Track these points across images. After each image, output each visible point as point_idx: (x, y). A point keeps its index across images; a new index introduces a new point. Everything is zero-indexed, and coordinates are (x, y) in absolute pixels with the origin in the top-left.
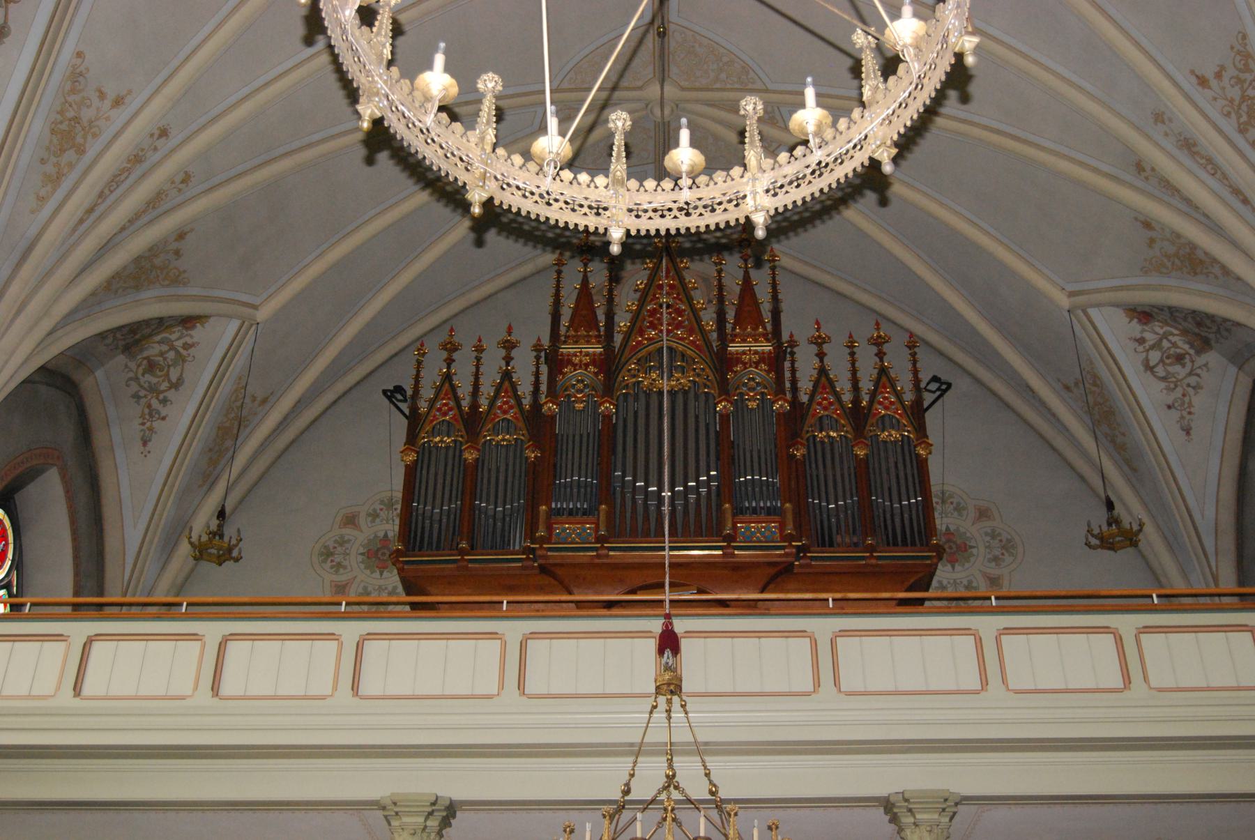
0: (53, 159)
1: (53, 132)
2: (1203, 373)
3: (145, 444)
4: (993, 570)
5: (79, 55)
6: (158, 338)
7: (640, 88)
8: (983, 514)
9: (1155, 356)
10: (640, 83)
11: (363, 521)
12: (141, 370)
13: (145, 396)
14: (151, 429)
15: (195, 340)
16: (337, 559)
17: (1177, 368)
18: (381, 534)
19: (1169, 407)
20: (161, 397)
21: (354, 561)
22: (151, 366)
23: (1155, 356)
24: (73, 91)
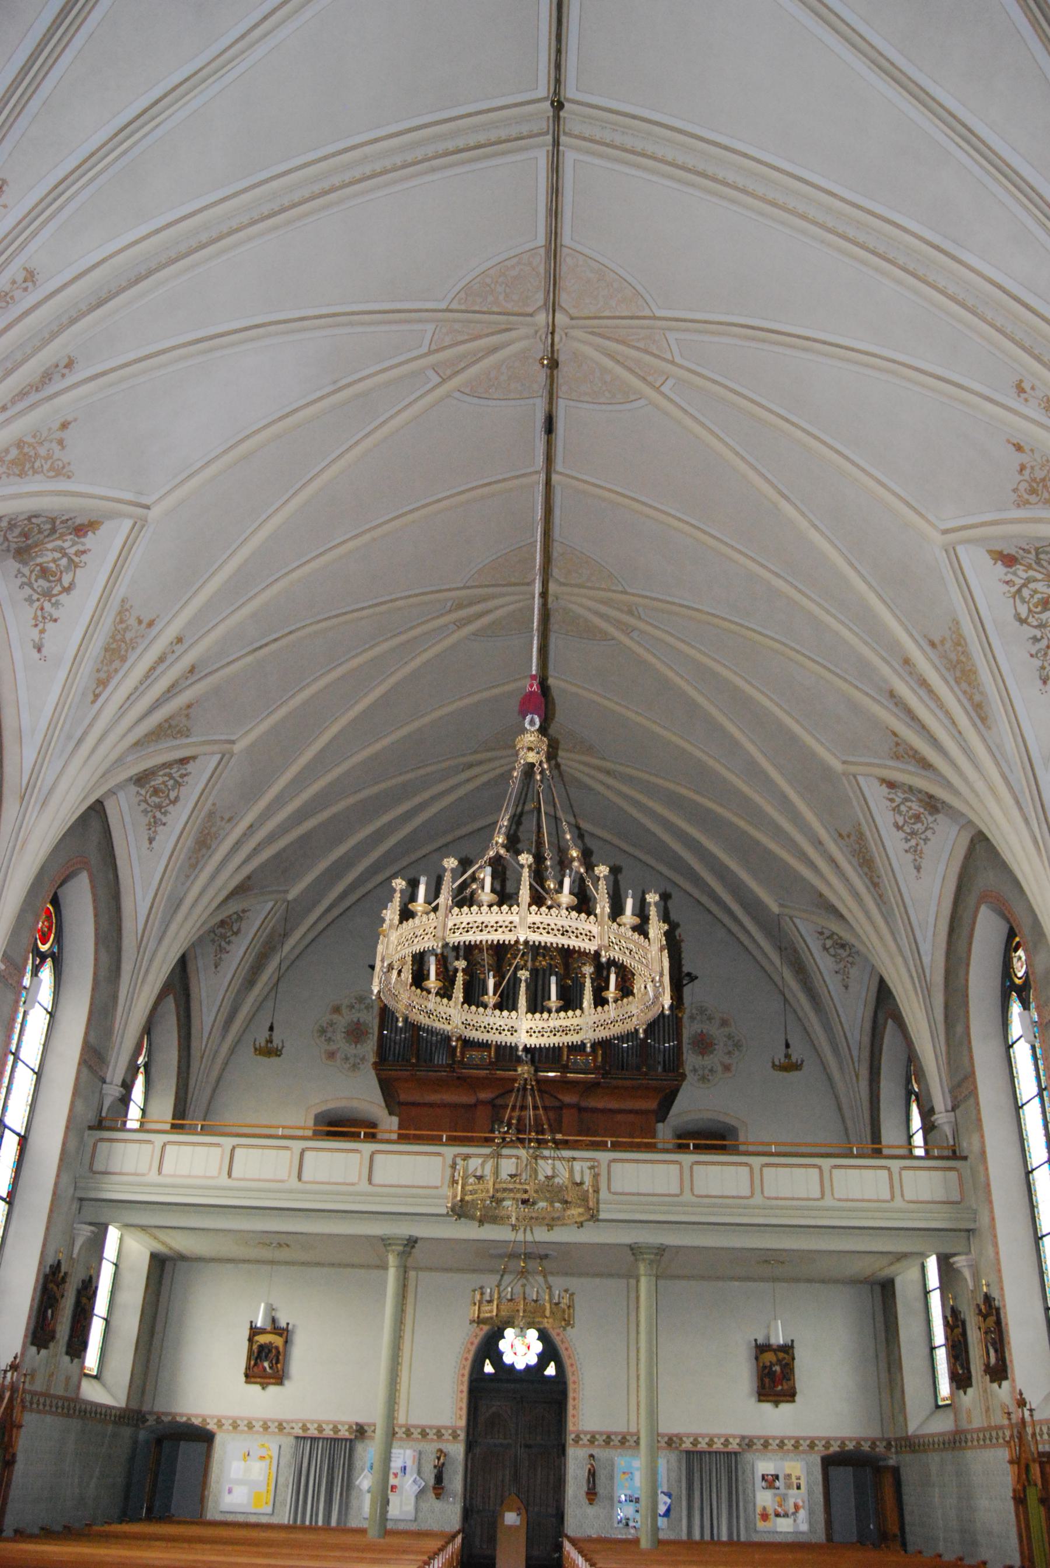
0: (105, 668)
1: (106, 650)
2: (856, 956)
3: (216, 967)
4: (727, 1060)
5: (214, 804)
6: (50, 546)
7: (531, 315)
8: (724, 1023)
9: (829, 943)
10: (530, 310)
11: (344, 1011)
12: (33, 577)
13: (38, 600)
14: (220, 958)
15: (88, 546)
16: (329, 1035)
17: (840, 951)
18: (355, 1020)
19: (906, 851)
20: (54, 600)
21: (339, 1036)
22: (44, 573)
23: (829, 943)
24: (122, 621)
